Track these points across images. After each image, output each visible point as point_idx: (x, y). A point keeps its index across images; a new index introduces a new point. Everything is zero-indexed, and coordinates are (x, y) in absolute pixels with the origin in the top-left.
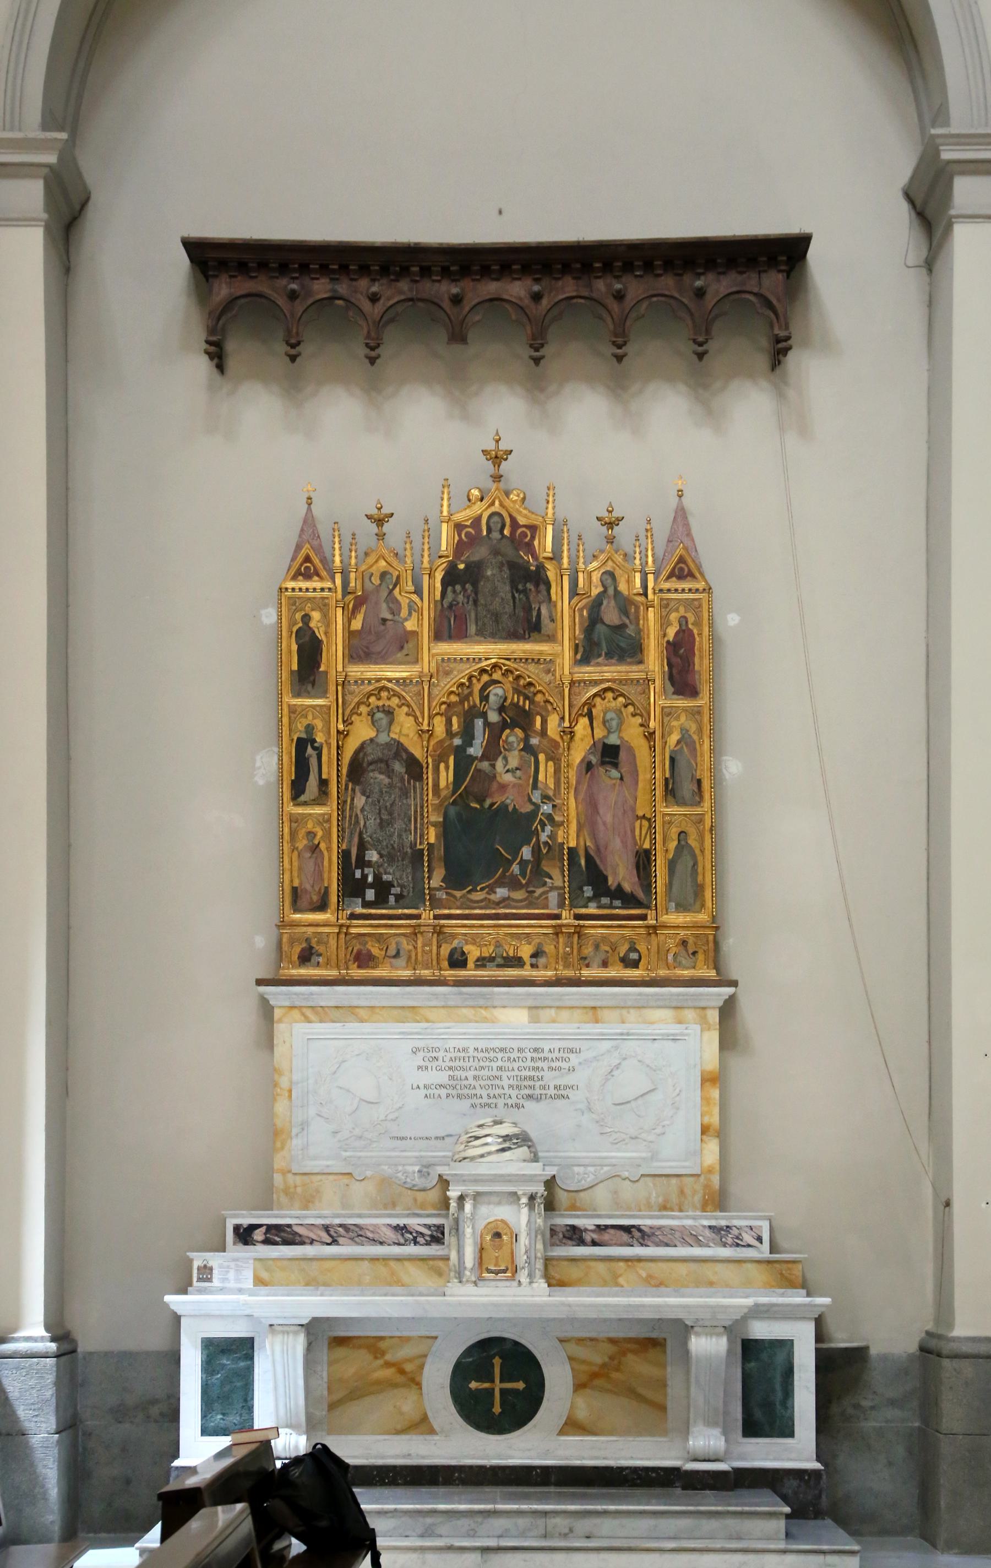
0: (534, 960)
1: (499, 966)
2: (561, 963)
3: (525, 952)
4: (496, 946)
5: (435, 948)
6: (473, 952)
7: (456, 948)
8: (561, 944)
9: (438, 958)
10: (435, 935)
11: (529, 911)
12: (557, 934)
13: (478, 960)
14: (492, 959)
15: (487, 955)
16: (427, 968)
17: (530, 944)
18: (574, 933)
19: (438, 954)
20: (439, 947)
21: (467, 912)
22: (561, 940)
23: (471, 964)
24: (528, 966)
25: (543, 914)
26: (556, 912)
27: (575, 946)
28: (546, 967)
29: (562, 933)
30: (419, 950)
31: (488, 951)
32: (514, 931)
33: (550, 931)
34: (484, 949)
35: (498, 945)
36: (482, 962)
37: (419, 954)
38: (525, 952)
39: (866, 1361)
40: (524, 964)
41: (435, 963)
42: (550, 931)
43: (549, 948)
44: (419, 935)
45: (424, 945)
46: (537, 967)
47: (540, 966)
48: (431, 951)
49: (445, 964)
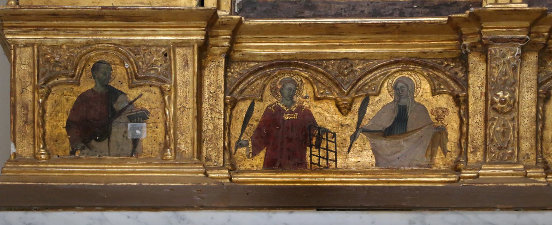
10: (532, 58)
37: (476, 121)
44: (474, 59)
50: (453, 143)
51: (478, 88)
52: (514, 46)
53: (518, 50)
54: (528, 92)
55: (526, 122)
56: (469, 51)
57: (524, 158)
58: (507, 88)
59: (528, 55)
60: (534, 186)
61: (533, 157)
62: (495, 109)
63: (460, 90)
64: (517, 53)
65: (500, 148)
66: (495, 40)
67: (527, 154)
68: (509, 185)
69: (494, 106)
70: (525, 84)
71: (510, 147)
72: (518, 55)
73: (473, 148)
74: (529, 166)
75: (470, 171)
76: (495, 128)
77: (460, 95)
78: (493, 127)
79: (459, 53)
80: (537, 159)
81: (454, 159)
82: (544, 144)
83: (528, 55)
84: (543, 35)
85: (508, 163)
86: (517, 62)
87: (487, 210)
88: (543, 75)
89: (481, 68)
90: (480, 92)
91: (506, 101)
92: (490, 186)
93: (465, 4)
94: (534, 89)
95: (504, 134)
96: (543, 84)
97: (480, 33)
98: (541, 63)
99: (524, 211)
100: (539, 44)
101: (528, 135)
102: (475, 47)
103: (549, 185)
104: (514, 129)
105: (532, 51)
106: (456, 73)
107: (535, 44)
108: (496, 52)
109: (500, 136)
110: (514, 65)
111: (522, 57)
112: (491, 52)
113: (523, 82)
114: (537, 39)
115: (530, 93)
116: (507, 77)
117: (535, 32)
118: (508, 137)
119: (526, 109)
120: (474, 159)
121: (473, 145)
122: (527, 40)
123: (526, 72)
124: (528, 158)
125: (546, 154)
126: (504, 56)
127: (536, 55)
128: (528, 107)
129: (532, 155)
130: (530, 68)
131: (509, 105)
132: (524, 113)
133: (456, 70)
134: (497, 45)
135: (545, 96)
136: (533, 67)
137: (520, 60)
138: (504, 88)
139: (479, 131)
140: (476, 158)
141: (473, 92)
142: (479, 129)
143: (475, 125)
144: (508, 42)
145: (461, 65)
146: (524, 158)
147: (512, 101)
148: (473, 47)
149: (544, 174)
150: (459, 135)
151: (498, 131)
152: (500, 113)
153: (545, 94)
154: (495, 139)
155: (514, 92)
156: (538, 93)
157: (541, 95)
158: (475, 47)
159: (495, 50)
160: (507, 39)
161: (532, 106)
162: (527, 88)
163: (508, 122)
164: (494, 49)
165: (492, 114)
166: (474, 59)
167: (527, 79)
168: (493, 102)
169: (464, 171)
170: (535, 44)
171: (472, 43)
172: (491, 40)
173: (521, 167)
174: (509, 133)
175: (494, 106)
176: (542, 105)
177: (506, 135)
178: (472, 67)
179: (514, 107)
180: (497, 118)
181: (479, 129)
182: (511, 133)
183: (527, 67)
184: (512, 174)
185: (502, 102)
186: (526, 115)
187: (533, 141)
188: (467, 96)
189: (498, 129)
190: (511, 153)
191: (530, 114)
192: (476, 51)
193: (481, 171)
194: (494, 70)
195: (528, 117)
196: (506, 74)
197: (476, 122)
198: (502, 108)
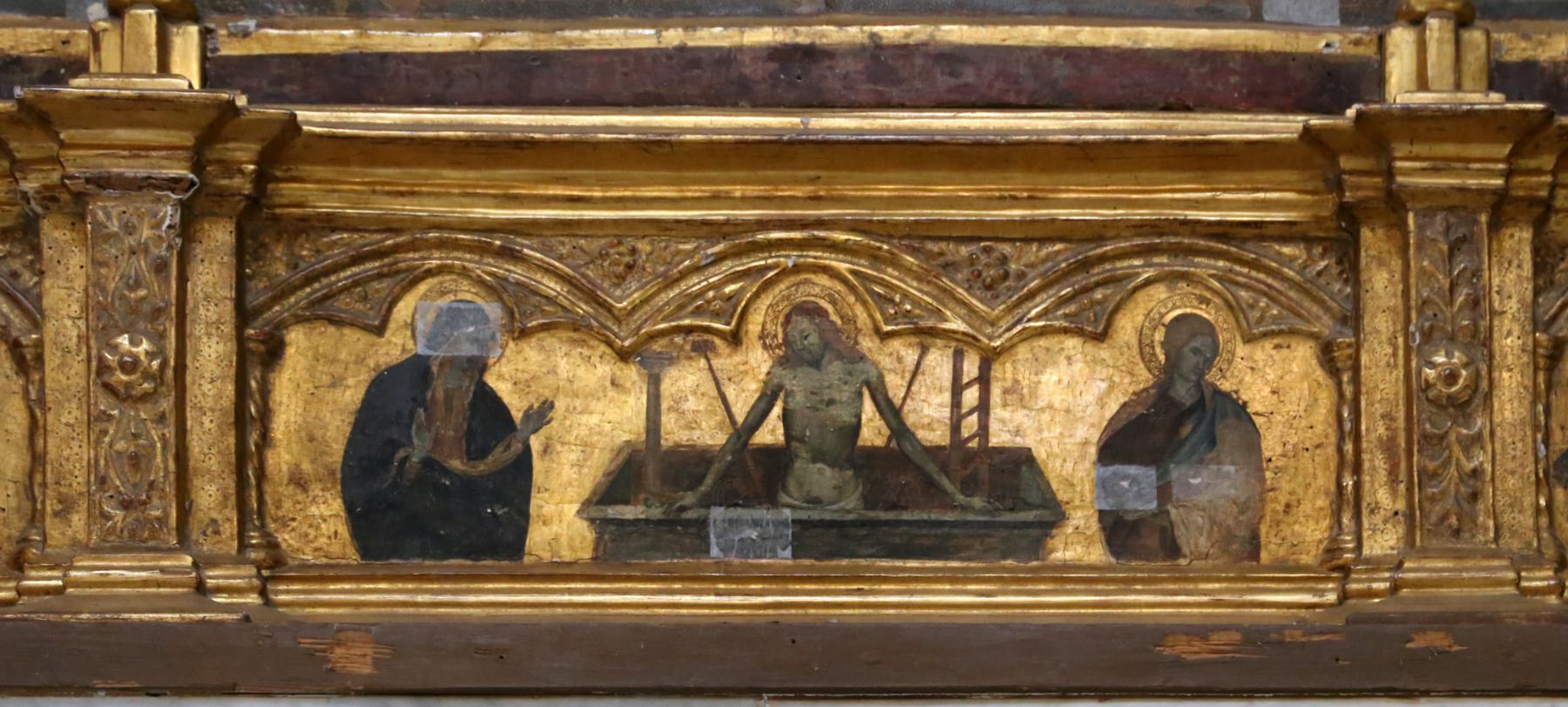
0: (1137, 486)
1: (825, 542)
2: (1381, 495)
3: (1060, 404)
4: (791, 356)
5: (212, 353)
6: (585, 411)
7: (416, 371)
8: (1380, 324)
9: (248, 464)
10: (220, 236)
11: (1087, 36)
12: (1339, 236)
13: (627, 476)
14: (749, 473)
15: (712, 435)
16: (133, 542)
17: (1096, 330)
18: (1501, 208)
19: (249, 418)
20: (258, 354)
21: (517, 39)
22: (1381, 283)
23: (559, 519)
24: (1080, 541)
25: (1211, 58)
26: (1332, 42)
27: (1510, 341)
28: (1244, 550)
29: (1394, 203)
30: (65, 373)
31: (702, 403)
32: (954, 199)
33: (1274, 202)
34: (685, 381)
35: (811, 345)
36: (658, 498)
37: (66, 417)
38: (1060, 404)
39: (310, 11)
40: (1053, 515)
41: (210, 495)
42: (1274, 202)
43: (1274, 381)
44: (54, 233)
45: (104, 317)
46: (1172, 549)
47: (1195, 538)
48: (177, 375)
49: (320, 522)
50: (11, 485)
51: (69, 323)
52: (158, 200)
53: (169, 213)
54: (209, 335)
55: (207, 425)
56: (39, 210)
57: (204, 533)
58: (141, 325)
59: (207, 226)
60: (203, 621)
61: (230, 529)
62: (107, 387)
63: (26, 324)
64: (167, 222)
65: (126, 505)
66: (103, 182)
67: (214, 521)
68: (135, 616)
69: (106, 378)
70: (202, 311)
71: (156, 501)
72: (170, 227)
73: (60, 502)
74: (218, 556)
75: (49, 573)
76: (111, 445)
77: (24, 341)
78: (107, 439)
79: (19, 215)
80: (242, 535)
81: (15, 533)
82: (268, 488)
83: (207, 226)
84: (241, 172)
85: (149, 550)
86: (170, 247)
87: (69, 695)
88: (261, 286)
89: (77, 260)
90: (75, 333)
91: (136, 361)
92: (81, 622)
93: (45, 67)
94: (228, 329)
95: (136, 461)
96: (262, 313)
97: (56, 161)
98: (245, 253)
99: (176, 699)
100: (233, 195)
101: (213, 463)
102: (54, 199)
103: (247, 619)
104: (164, 448)
105: (216, 215)
106: (15, 275)
107: (221, 195)
108: (108, 216)
109: (127, 469)
110: (160, 257)
111: (187, 229)
112: (94, 216)
113: (196, 307)
114: (225, 182)
115: (215, 339)
116: (142, 293)
117: (219, 161)
118: (149, 471)
119: (206, 387)
120: (63, 534)
121: (60, 493)
122: (192, 184)
123: (204, 278)
124: (217, 532)
125: (275, 520)
126: (129, 229)
127: (231, 227)
128: (212, 381)
129: (227, 525)
130: (215, 267)
131: (147, 376)
132: (200, 397)
133: (16, 265)
134: (109, 198)
135: (262, 348)
136: (221, 264)
137: (179, 241)
138: (132, 324)
139: (76, 449)
140: (70, 532)
141: (57, 333)
142: (75, 444)
143: (64, 431)
144: (140, 188)
145: (27, 248)
146: (204, 533)
147: (155, 364)
148: (49, 197)
149: (256, 582)
150: (28, 459)
151: (119, 453)
152: (124, 400)
153: (262, 342)
154: (112, 474)
155: (162, 336)
156: (241, 339)
157: (252, 345)
158: (54, 199)
159: (108, 211)
160: (135, 178)
161: (223, 378)
162: (208, 324)
163: (149, 424)
164: (104, 209)
165: (104, 403)
166: (57, 234)
167: (207, 298)
168: (103, 368)
169: (33, 573)
170: (221, 195)
171: (46, 187)
172: (88, 180)
173: (188, 560)
174: (152, 456)
175: (106, 378)
176: (258, 374)
177: (143, 466)
178: (51, 259)
179: (162, 383)
180: (115, 412)
181: (75, 444)
182: (159, 459)
183: (206, 264)
184: (159, 584)
185: (123, 367)
186: (208, 403)
187: (231, 483)
188: (40, 344)
189: (120, 445)
190: (158, 519)
191: (216, 402)
192: (60, 210)
193: (73, 574)
194: (103, 271)
195: (213, 410)
196: (138, 284)
197: (67, 425)
198: (128, 385)
